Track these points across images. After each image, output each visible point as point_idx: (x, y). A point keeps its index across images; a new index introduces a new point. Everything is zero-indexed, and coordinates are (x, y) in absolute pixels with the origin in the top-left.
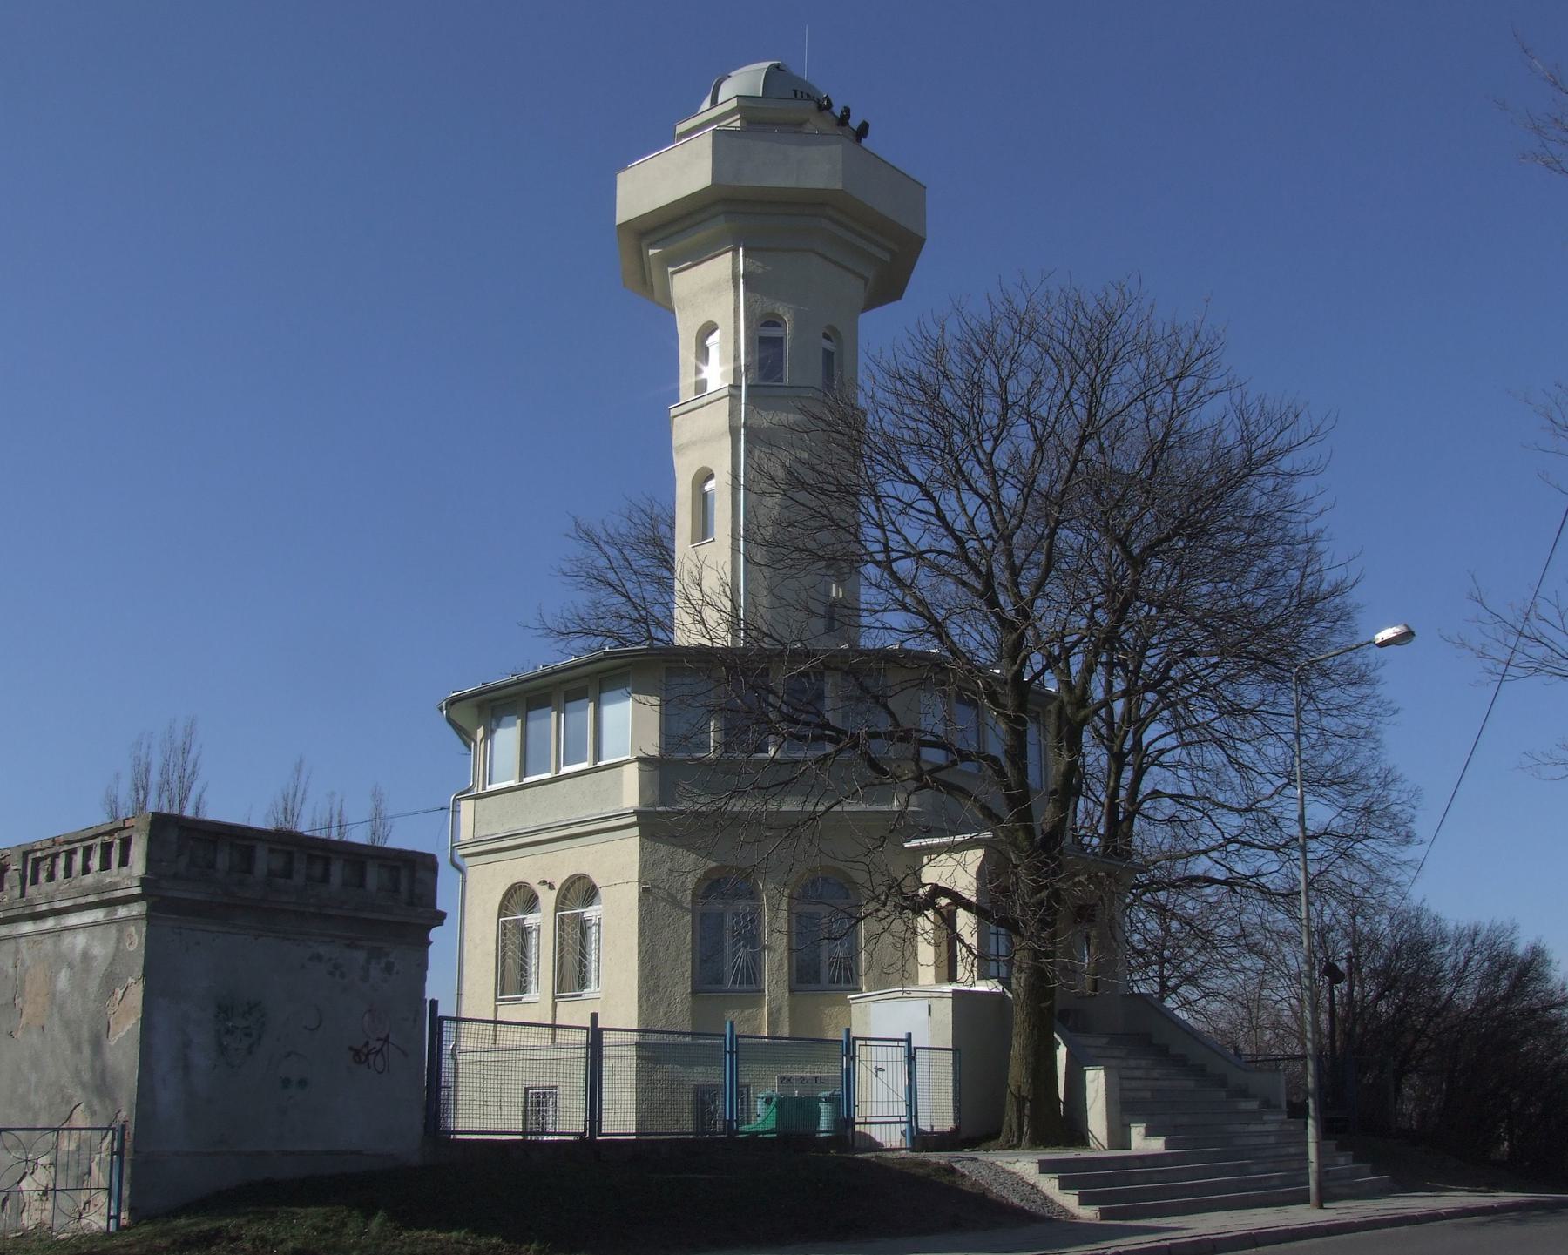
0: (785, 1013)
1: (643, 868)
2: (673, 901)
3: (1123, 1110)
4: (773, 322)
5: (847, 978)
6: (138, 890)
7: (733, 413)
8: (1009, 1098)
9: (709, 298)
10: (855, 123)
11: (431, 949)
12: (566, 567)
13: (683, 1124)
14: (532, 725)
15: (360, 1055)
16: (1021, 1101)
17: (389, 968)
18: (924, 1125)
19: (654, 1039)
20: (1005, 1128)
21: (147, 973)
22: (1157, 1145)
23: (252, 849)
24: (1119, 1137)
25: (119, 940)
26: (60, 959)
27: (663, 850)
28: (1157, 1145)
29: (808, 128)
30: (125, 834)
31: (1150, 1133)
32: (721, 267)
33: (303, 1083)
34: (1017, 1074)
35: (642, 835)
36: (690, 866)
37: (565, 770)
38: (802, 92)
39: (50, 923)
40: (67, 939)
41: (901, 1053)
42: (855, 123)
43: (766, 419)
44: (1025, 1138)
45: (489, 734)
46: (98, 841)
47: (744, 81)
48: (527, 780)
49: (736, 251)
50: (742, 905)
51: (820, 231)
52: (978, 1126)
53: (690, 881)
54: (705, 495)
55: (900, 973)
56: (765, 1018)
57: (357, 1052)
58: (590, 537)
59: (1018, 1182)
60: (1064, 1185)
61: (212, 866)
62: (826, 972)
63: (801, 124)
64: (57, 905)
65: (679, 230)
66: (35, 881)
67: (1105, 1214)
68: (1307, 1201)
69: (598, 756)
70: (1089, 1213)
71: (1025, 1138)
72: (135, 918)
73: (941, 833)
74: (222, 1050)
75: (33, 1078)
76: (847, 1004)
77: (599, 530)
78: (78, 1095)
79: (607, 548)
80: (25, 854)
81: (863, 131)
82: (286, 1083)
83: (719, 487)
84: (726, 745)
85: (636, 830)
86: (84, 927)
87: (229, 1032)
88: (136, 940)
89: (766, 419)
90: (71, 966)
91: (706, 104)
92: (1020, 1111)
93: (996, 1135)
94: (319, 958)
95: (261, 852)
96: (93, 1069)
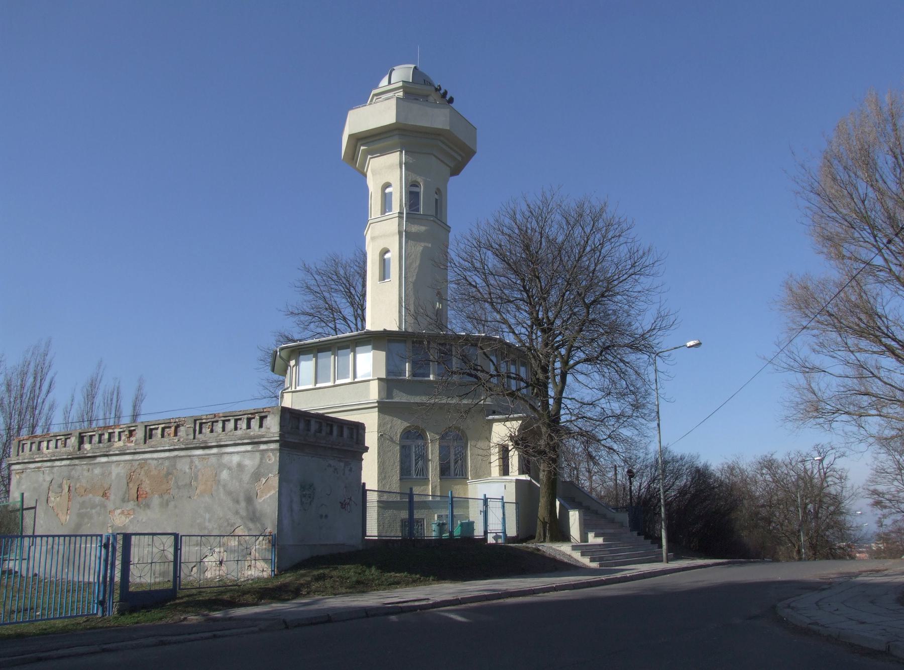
0: (438, 488)
1: (380, 426)
2: (391, 440)
3: (585, 527)
4: (415, 184)
5: (462, 475)
6: (278, 438)
7: (400, 225)
8: (539, 523)
9: (386, 172)
10: (448, 97)
11: (363, 462)
12: (298, 284)
13: (396, 533)
14: (320, 361)
15: (343, 505)
16: (544, 523)
17: (351, 470)
18: (133, 537)
19: (385, 498)
20: (537, 534)
21: (281, 472)
22: (600, 540)
23: (309, 421)
24: (584, 538)
25: (261, 459)
26: (222, 466)
27: (388, 418)
28: (600, 540)
29: (431, 99)
30: (263, 414)
31: (596, 536)
32: (394, 159)
33: (326, 516)
34: (542, 512)
35: (379, 411)
36: (399, 425)
37: (338, 382)
38: (427, 82)
39: (215, 451)
40: (226, 459)
41: (500, 504)
42: (448, 97)
43: (415, 228)
44: (548, 539)
45: (297, 364)
46: (246, 416)
47: (401, 74)
48: (318, 386)
49: (401, 152)
50: (420, 442)
51: (435, 147)
52: (527, 532)
53: (399, 431)
54: (384, 260)
55: (482, 473)
56: (430, 488)
57: (342, 504)
58: (308, 271)
59: (564, 554)
60: (583, 554)
61: (298, 428)
62: (454, 469)
63: (427, 96)
64: (222, 443)
65: (375, 140)
66: (200, 432)
67: (601, 565)
68: (662, 561)
69: (355, 376)
70: (595, 565)
71: (548, 539)
72: (272, 450)
73: (500, 414)
74: (302, 503)
75: (207, 516)
76: (466, 484)
77: (313, 267)
78: (239, 522)
79: (316, 276)
80: (195, 421)
81: (451, 100)
82: (321, 516)
83: (393, 256)
84: (414, 374)
85: (376, 409)
86: (238, 453)
87: (304, 496)
88: (273, 459)
89: (415, 228)
90: (230, 469)
91: (385, 82)
92: (544, 528)
93: (534, 538)
94: (330, 466)
95: (313, 422)
96: (247, 510)
